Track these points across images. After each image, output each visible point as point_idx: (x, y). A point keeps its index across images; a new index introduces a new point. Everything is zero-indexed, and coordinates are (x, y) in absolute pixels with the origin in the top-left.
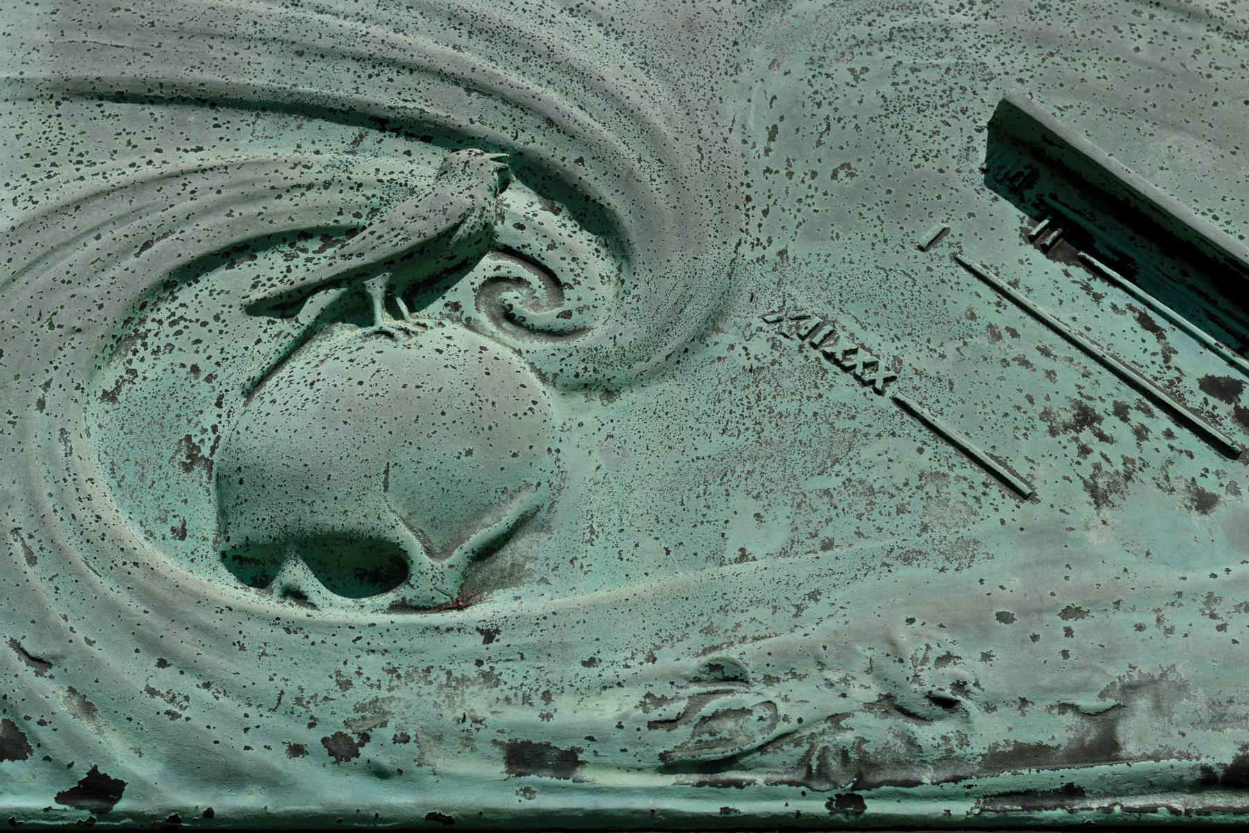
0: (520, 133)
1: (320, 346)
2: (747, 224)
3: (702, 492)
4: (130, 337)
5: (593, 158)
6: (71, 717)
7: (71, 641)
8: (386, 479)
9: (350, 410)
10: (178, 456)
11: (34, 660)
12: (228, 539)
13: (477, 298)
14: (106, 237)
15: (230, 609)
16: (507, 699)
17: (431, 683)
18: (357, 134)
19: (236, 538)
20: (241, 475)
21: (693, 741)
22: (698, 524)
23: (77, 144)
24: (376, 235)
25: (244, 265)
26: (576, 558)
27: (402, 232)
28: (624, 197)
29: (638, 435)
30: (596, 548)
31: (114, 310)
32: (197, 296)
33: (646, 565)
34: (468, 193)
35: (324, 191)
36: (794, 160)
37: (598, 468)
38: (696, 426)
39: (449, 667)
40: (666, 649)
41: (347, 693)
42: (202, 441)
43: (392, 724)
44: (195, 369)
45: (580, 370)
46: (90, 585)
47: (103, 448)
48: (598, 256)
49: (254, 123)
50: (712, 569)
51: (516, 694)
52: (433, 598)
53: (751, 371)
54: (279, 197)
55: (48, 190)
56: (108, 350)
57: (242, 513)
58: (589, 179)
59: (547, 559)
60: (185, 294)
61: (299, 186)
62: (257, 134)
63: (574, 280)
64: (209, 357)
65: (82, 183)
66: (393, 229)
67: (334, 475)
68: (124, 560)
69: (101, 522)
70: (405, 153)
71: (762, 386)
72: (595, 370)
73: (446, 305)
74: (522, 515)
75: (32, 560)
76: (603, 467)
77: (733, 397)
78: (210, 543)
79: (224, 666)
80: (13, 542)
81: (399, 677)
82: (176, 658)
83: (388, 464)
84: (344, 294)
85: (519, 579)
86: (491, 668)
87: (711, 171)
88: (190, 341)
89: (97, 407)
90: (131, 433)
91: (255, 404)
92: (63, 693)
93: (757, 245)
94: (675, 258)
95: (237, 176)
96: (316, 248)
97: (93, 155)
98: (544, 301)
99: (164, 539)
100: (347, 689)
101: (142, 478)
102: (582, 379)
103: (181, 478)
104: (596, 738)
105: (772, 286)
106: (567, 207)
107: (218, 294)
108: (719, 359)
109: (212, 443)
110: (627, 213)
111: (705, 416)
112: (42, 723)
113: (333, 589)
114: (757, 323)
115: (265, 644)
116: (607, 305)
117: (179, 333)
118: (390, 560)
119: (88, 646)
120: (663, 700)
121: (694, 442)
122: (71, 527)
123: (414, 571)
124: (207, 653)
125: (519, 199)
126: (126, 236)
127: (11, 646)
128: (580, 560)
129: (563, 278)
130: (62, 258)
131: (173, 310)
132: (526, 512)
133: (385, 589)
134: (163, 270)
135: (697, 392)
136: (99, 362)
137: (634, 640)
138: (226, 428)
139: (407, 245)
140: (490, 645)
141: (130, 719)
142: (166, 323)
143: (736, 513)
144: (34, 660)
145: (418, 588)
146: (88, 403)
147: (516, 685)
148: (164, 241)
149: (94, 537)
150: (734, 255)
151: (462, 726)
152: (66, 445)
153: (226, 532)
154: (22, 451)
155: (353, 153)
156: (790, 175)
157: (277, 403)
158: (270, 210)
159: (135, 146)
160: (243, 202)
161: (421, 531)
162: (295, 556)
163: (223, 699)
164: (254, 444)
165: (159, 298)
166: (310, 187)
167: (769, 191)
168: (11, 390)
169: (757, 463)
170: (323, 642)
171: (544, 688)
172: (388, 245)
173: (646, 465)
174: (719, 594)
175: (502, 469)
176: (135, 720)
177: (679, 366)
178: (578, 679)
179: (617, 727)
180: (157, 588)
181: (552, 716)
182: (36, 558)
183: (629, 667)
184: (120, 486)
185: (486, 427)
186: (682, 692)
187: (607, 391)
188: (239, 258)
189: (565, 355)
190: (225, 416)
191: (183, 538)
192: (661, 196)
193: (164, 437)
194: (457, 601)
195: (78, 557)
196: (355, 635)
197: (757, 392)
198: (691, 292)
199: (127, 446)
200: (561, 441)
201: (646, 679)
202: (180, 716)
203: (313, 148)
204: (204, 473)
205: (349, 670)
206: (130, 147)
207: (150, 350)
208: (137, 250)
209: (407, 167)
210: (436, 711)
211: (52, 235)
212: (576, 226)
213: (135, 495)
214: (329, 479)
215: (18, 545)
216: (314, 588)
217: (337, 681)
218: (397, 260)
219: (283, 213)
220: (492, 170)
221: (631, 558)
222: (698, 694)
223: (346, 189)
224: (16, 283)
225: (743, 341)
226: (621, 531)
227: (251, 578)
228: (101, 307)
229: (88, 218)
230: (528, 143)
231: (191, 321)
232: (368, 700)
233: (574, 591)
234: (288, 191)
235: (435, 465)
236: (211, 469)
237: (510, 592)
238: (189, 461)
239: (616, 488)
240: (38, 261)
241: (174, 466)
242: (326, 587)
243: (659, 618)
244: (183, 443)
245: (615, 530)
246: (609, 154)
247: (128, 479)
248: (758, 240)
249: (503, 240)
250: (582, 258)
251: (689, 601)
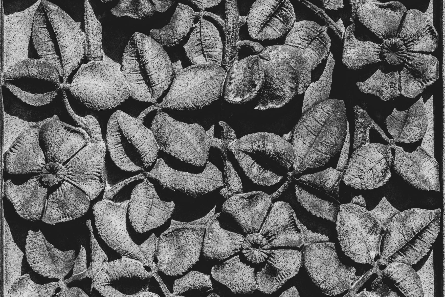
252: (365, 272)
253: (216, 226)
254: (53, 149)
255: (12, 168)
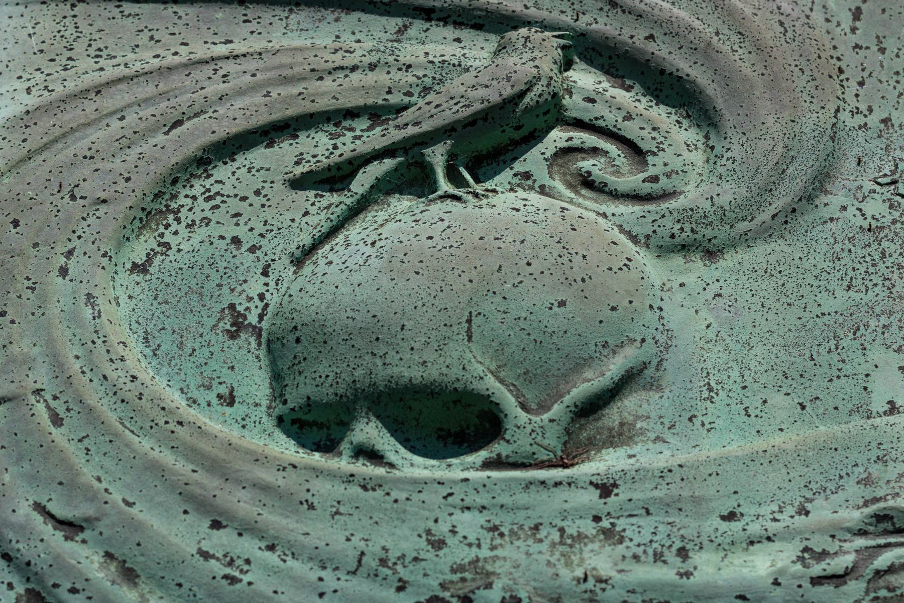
0: (581, 15)
1: (376, 215)
2: (843, 93)
3: (833, 347)
4: (161, 212)
5: (665, 34)
6: (109, 584)
7: (106, 503)
8: (469, 329)
9: (421, 262)
10: (221, 324)
11: (62, 523)
12: (285, 402)
13: (550, 167)
14: (131, 118)
15: (295, 467)
16: (636, 557)
17: (541, 541)
18: (401, 24)
19: (295, 398)
20: (298, 334)
21: (868, 598)
22: (835, 379)
23: (95, 40)
24: (434, 104)
25: (285, 144)
26: (695, 416)
27: (462, 100)
28: (704, 68)
29: (750, 294)
30: (717, 405)
31: (143, 183)
32: (233, 173)
33: (778, 420)
34: (532, 64)
35: (370, 73)
36: (884, 37)
37: (708, 326)
38: (816, 283)
39: (560, 524)
40: (819, 501)
41: (441, 553)
42: (247, 309)
43: (498, 585)
44: (236, 241)
45: (676, 231)
46: (127, 445)
47: (134, 319)
48: (680, 127)
49: (287, 18)
50: (857, 421)
51: (645, 552)
52: (534, 453)
53: (869, 230)
54: (321, 78)
55: (65, 80)
56: (137, 223)
57: (300, 373)
58: (664, 53)
59: (660, 417)
60: (221, 172)
61: (342, 68)
62: (290, 27)
63: (657, 147)
64: (251, 229)
65: (102, 73)
66: (452, 98)
67: (408, 325)
68: (165, 419)
69: (138, 383)
70: (455, 40)
71: (885, 244)
72: (692, 230)
73: (515, 175)
74: (627, 371)
75: (57, 421)
76: (714, 325)
77: (853, 255)
78: (264, 408)
79: (291, 526)
80: (35, 403)
81: (502, 535)
82: (232, 518)
83: (470, 313)
84: (400, 164)
85: (630, 438)
86: (612, 524)
87: (796, 43)
88: (229, 215)
89: (124, 277)
90: (166, 303)
91: (307, 269)
92: (98, 559)
93: (857, 113)
94: (770, 120)
95: (276, 60)
96: (365, 127)
97: (113, 50)
98: (625, 169)
99: (209, 405)
100: (440, 549)
101: (181, 346)
102: (677, 240)
103: (226, 345)
104: (748, 596)
105: (880, 151)
106: (639, 83)
107: (258, 171)
108: (832, 219)
109: (259, 311)
110: (710, 82)
111: (824, 274)
112: (73, 591)
113: (413, 450)
114: (869, 185)
115: (339, 502)
116: (697, 170)
117: (217, 207)
118: (478, 417)
119: (127, 508)
120: (823, 555)
121: (816, 299)
122: (103, 388)
123: (509, 425)
124: (270, 513)
126: (154, 115)
127: (35, 509)
128: (700, 418)
129: (644, 146)
130: (83, 138)
131: (208, 187)
132: (632, 368)
133: (474, 448)
134: (195, 145)
135: (812, 251)
136: (127, 233)
137: (779, 493)
138: (275, 295)
139: (468, 112)
140: (608, 500)
141: (180, 585)
142: (201, 200)
143: (876, 366)
144: (62, 523)
146: (116, 273)
147: (644, 542)
148: (196, 120)
149: (128, 396)
150: (834, 120)
151: (583, 587)
152: (93, 308)
153: (282, 395)
154: (43, 314)
155: (398, 41)
156: (882, 51)
157: (334, 264)
158: (311, 91)
159: (158, 41)
160: (281, 84)
161: (513, 385)
162: (367, 414)
163: (290, 562)
164: (311, 302)
165: (192, 175)
166: (354, 69)
167: (862, 64)
168: (29, 258)
169: (892, 318)
170: (408, 499)
171: (678, 544)
172: (448, 112)
173: (764, 322)
174: (874, 444)
175: (601, 322)
176: (186, 586)
177: (788, 226)
178: (718, 534)
179: (773, 584)
180: (205, 446)
181: (692, 574)
182: (62, 419)
183: (778, 520)
184: (155, 355)
185: (579, 279)
186: (846, 546)
187: (708, 252)
188: (279, 137)
189: (657, 217)
190: (272, 284)
191: (231, 403)
192: (746, 65)
193: (204, 306)
194: (562, 458)
195: (112, 418)
196: (445, 491)
197: (880, 250)
198: (792, 153)
199: (161, 316)
200: (662, 300)
201: (801, 533)
202: (241, 580)
203: (353, 38)
204: (252, 340)
205: (443, 529)
206: (153, 42)
207: (183, 224)
208: (166, 129)
209: (459, 52)
210: (551, 571)
211: (71, 116)
212: (651, 101)
213: (173, 363)
214: (402, 329)
215: (41, 408)
216: (390, 448)
217: (428, 540)
218: (459, 128)
219: (325, 93)
220: (555, 45)
221: (760, 414)
222: (867, 548)
223: (393, 71)
224: (31, 161)
225: (856, 202)
226: (744, 388)
227: (314, 444)
228: (128, 180)
229: (110, 101)
230: (590, 24)
231: (228, 196)
232: (466, 561)
233: (698, 448)
234: (330, 73)
235: (524, 315)
236: (259, 336)
237: (622, 452)
238: (234, 328)
239: (732, 345)
240: (56, 140)
241: (217, 334)
242: (405, 447)
243: (806, 470)
244: (226, 311)
245: (737, 387)
246: (682, 29)
247: (164, 347)
248: (857, 108)
249: (572, 114)
250: (664, 127)
251: (839, 451)
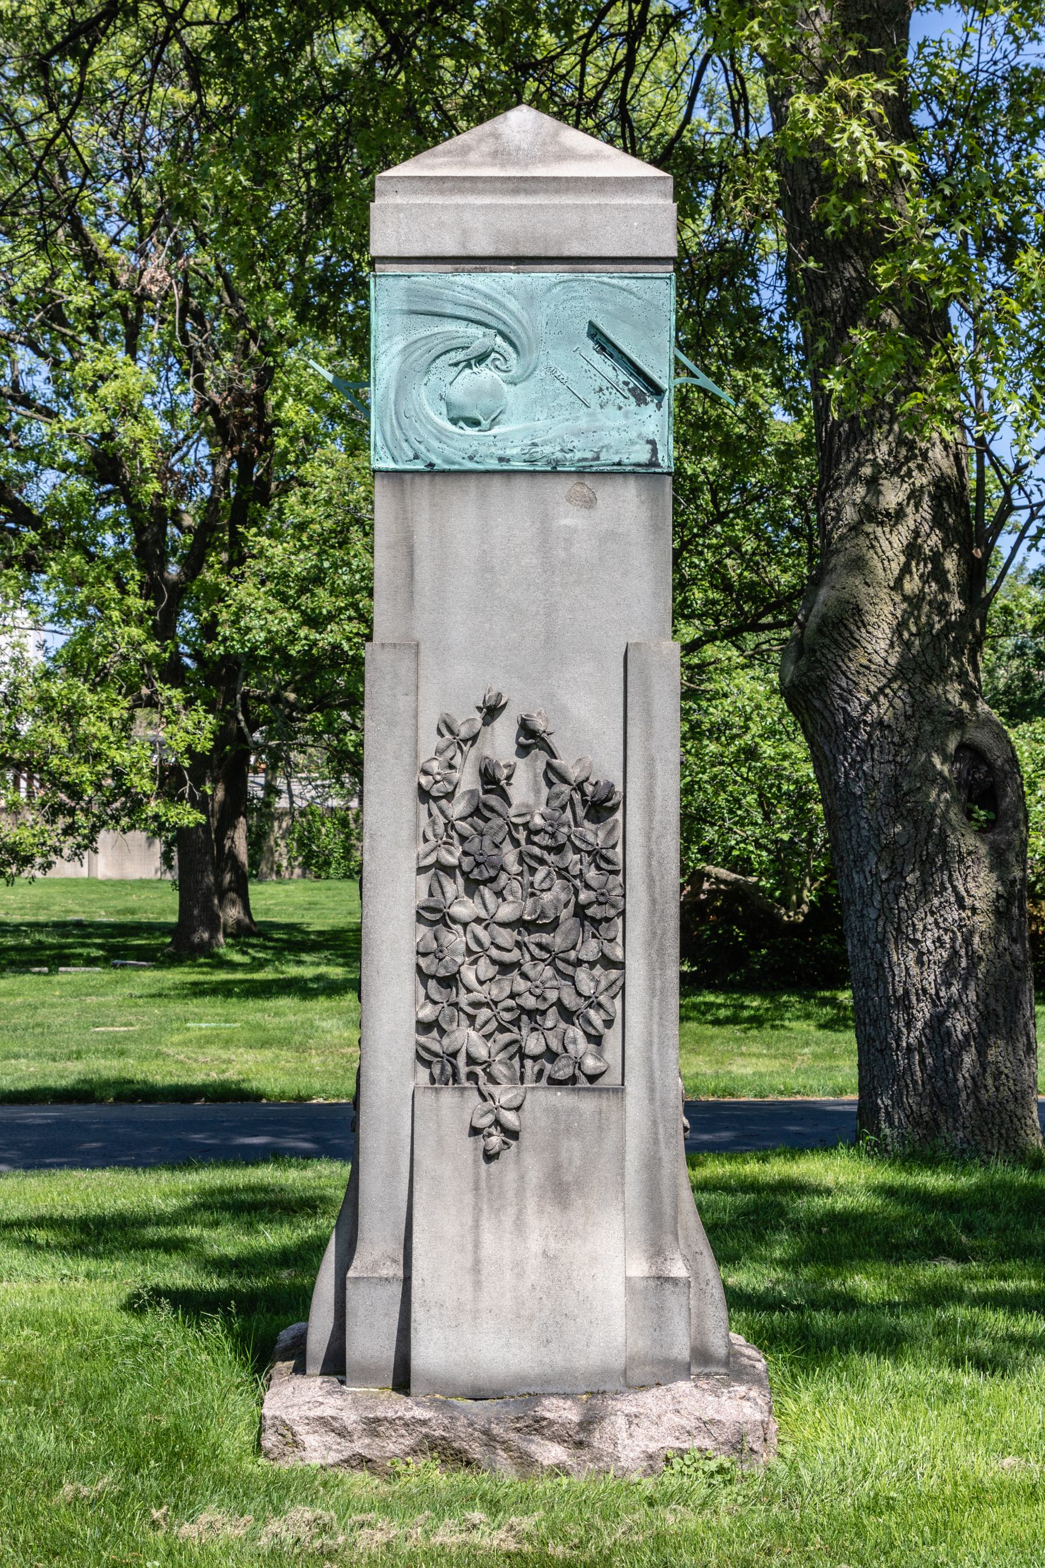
1: (463, 374)
125: (499, 339)
145: (482, 427)
211: (412, 349)
252: (820, 1204)
253: (518, 978)
254: (441, 941)
255: (421, 950)
